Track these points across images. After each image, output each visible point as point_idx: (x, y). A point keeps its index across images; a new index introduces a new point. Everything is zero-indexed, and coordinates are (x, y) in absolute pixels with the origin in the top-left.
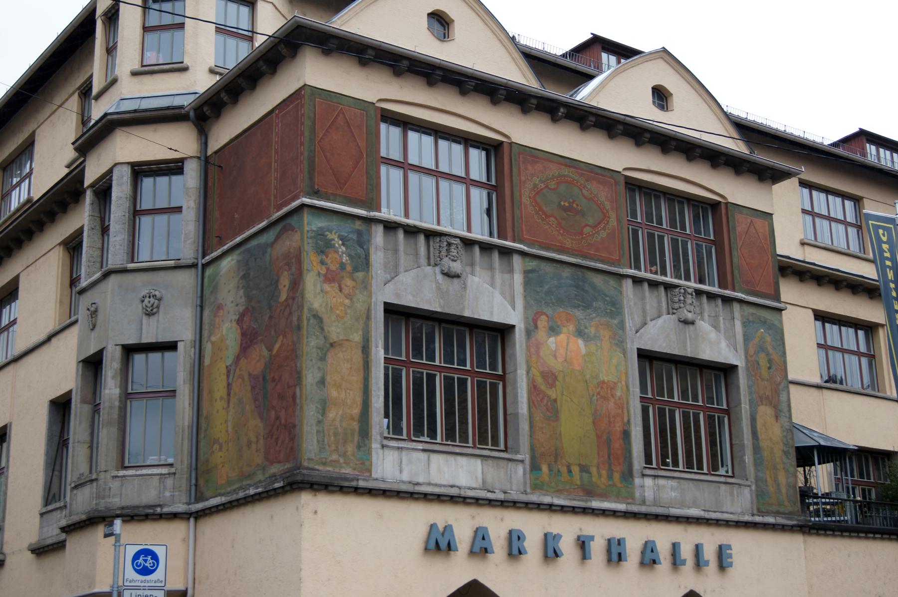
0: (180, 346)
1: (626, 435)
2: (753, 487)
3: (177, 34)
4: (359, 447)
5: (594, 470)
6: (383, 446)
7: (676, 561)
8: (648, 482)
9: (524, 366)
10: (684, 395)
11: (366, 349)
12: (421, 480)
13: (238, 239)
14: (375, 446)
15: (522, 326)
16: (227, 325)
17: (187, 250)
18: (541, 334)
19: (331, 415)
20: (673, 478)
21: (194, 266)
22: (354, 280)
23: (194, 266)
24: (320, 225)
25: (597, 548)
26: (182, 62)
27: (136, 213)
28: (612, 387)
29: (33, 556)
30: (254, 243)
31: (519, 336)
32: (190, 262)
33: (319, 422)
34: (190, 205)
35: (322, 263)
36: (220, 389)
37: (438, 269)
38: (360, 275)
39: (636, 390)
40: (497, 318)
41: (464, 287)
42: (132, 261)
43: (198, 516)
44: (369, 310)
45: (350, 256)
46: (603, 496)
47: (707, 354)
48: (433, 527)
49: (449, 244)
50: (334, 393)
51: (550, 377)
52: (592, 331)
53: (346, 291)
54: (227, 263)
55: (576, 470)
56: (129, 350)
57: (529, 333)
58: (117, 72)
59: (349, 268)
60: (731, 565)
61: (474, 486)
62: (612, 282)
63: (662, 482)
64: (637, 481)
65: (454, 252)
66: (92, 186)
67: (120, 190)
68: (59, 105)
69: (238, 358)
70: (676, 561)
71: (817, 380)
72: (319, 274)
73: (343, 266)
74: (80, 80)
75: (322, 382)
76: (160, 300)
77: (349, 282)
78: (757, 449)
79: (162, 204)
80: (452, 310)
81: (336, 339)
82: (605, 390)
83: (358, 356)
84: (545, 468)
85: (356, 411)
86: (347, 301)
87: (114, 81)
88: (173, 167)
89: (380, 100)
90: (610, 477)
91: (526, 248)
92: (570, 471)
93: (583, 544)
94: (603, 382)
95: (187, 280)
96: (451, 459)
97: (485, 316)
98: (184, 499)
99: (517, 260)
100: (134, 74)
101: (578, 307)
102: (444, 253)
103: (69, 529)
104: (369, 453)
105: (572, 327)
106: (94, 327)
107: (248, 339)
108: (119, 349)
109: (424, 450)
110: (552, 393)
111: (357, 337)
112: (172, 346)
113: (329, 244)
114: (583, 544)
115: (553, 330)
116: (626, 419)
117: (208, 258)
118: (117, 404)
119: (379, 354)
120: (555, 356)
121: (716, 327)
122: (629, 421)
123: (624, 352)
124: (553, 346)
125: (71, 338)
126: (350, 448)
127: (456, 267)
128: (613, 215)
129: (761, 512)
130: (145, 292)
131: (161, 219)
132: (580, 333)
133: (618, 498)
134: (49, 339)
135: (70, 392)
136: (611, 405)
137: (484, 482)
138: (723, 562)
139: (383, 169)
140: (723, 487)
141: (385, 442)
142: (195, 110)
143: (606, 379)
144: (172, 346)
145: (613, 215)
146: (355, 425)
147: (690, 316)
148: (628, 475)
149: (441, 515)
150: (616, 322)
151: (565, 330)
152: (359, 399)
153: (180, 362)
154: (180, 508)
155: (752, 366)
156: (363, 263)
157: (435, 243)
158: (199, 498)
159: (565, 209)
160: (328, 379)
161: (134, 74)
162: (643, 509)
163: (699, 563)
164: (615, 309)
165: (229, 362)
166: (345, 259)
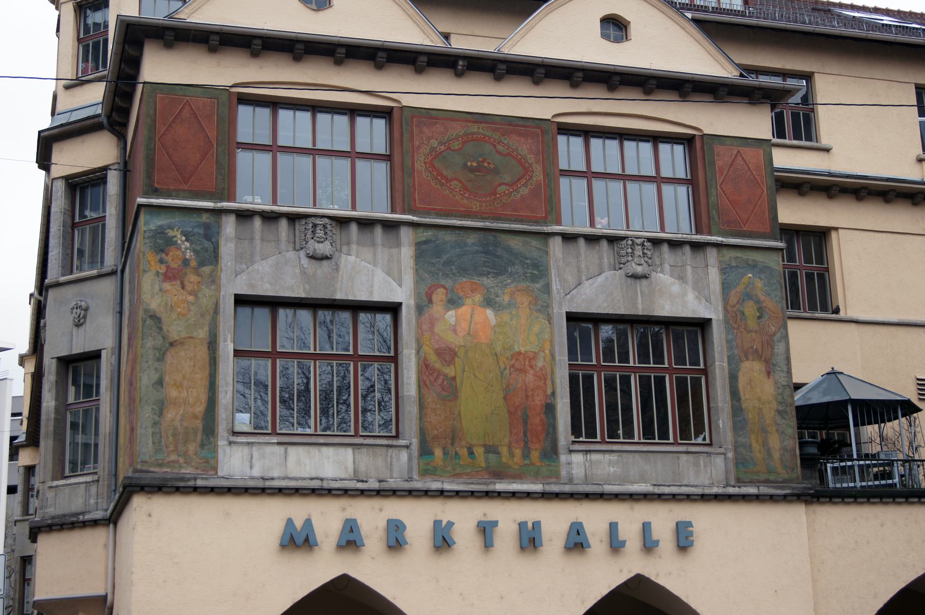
1: (550, 409)
2: (730, 455)
4: (202, 446)
5: (504, 450)
6: (230, 443)
7: (616, 545)
8: (577, 458)
11: (212, 345)
12: (275, 474)
14: (222, 443)
15: (412, 302)
18: (437, 308)
25: (506, 533)
28: (531, 358)
33: (155, 424)
35: (161, 261)
38: (207, 270)
39: (562, 358)
41: (337, 269)
44: (217, 305)
45: (194, 251)
47: (666, 309)
49: (315, 226)
51: (448, 354)
53: (189, 287)
55: (479, 451)
57: (420, 309)
59: (194, 263)
62: (534, 242)
63: (595, 457)
64: (563, 458)
65: (320, 233)
70: (616, 545)
73: (186, 262)
75: (160, 383)
77: (193, 278)
78: (737, 410)
83: (202, 353)
84: (438, 452)
85: (200, 409)
86: (191, 298)
90: (526, 454)
91: (415, 218)
92: (471, 453)
93: (486, 530)
94: (520, 353)
96: (314, 450)
101: (487, 274)
102: (309, 235)
105: (478, 298)
109: (278, 443)
110: (450, 371)
113: (170, 242)
114: (486, 530)
115: (453, 302)
120: (455, 331)
121: (682, 278)
122: (553, 393)
123: (549, 319)
126: (192, 447)
127: (324, 248)
129: (740, 482)
133: (536, 477)
136: (530, 377)
140: (684, 457)
143: (523, 350)
146: (199, 424)
147: (639, 270)
148: (551, 452)
151: (468, 301)
152: (204, 397)
155: (733, 317)
156: (213, 257)
157: (300, 226)
159: (472, 170)
162: (567, 489)
163: (649, 546)
166: (189, 254)
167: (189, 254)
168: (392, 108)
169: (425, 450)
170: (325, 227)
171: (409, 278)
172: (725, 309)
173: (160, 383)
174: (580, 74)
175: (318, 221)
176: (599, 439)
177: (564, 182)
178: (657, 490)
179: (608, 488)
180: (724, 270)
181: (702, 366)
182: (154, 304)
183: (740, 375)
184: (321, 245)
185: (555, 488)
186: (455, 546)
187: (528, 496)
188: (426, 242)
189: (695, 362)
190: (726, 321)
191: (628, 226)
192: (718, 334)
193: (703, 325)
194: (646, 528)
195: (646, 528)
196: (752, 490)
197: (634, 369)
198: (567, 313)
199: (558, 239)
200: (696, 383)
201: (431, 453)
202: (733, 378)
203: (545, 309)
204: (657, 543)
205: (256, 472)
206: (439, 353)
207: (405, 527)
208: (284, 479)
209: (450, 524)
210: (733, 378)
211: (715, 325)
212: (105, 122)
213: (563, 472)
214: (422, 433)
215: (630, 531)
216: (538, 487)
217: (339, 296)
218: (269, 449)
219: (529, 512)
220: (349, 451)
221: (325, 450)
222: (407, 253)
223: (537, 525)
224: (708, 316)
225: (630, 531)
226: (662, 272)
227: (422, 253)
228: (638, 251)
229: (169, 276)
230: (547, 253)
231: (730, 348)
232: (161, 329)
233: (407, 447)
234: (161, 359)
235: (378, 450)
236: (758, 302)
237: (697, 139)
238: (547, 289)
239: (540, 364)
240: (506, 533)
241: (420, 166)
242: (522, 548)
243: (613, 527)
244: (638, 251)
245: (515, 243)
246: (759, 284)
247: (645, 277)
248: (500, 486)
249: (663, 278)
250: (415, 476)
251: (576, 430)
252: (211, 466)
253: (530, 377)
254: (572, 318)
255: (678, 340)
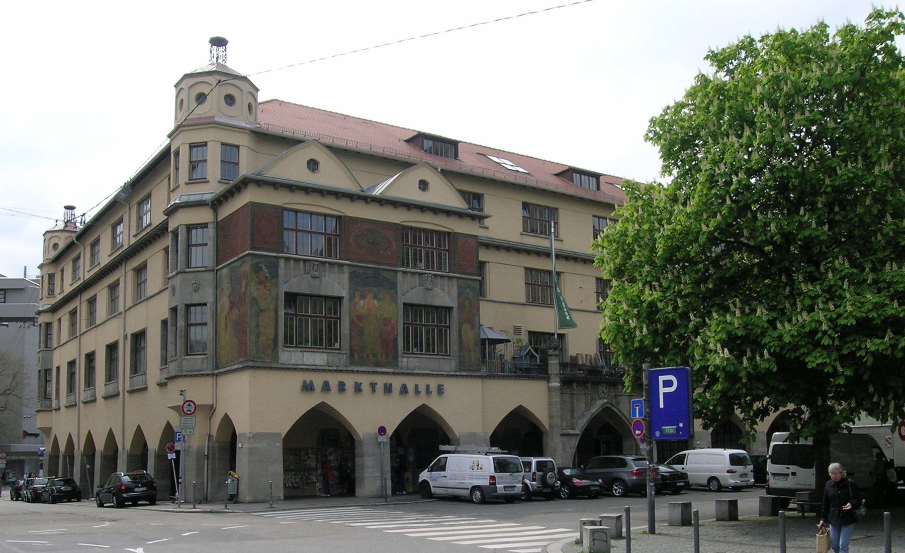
0: (208, 304)
1: (396, 340)
2: (458, 360)
3: (204, 164)
4: (273, 351)
5: (379, 355)
6: (283, 351)
7: (417, 392)
8: (405, 360)
9: (348, 313)
10: (427, 320)
11: (276, 311)
12: (299, 363)
13: (228, 262)
14: (280, 350)
15: (348, 296)
16: (225, 298)
17: (209, 262)
18: (357, 299)
19: (261, 339)
20: (417, 357)
21: (213, 270)
22: (272, 283)
23: (213, 270)
24: (256, 261)
25: (380, 387)
26: (206, 178)
27: (189, 246)
28: (389, 320)
29: (158, 387)
30: (233, 265)
31: (346, 302)
32: (211, 269)
33: (256, 342)
34: (211, 243)
35: (257, 277)
36: (223, 325)
37: (308, 275)
38: (273, 281)
39: (401, 321)
40: (336, 294)
41: (321, 282)
42: (188, 268)
43: (217, 375)
44: (277, 295)
45: (269, 273)
46: (383, 366)
47: (438, 303)
48: (305, 382)
49: (314, 264)
50: (262, 330)
51: (360, 318)
52: (381, 296)
53: (267, 288)
54: (225, 271)
55: (371, 356)
56: (188, 306)
57: (351, 299)
58: (180, 182)
59: (269, 278)
60: (443, 393)
61: (323, 364)
62: (392, 274)
63: (411, 359)
64: (400, 359)
65: (316, 267)
66: (171, 232)
67: (182, 237)
68: (127, 274)
69: (228, 313)
70: (417, 392)
71: (524, 301)
72: (256, 282)
73: (266, 278)
74: (168, 174)
75: (258, 326)
76: (199, 285)
77: (269, 284)
78: (461, 342)
79: (200, 242)
80: (315, 292)
81: (263, 308)
82: (387, 321)
83: (273, 315)
84: (356, 356)
85: (272, 337)
86: (268, 292)
87: (178, 186)
88: (204, 226)
89: (283, 204)
90: (387, 358)
91: (350, 263)
92: (368, 357)
93: (373, 386)
94: (386, 318)
95: (210, 276)
96: (312, 354)
97: (330, 294)
98: (211, 368)
99: (346, 269)
100: (186, 184)
101: (375, 286)
102: (311, 268)
103: (170, 378)
104: (277, 353)
105: (371, 295)
106: (174, 295)
107: (232, 305)
108: (184, 306)
109: (301, 351)
110: (361, 325)
111: (272, 307)
112: (205, 304)
113: (261, 269)
114: (373, 386)
115: (363, 297)
116: (396, 333)
117: (218, 267)
118: (183, 329)
119: (282, 312)
120: (363, 309)
121: (443, 290)
122: (397, 335)
123: (397, 304)
124: (362, 305)
125: (166, 295)
126: (270, 352)
127: (316, 274)
128: (394, 243)
129: (460, 370)
130: (193, 282)
131: (200, 248)
132: (375, 298)
133: (390, 366)
134: (160, 292)
135: (177, 306)
136: (389, 328)
137: (328, 362)
138: (440, 390)
139: (285, 232)
140: (442, 361)
141: (284, 349)
142: (211, 202)
143: (387, 316)
144: (205, 304)
145: (394, 243)
146: (271, 343)
147: (430, 287)
148: (396, 357)
149: (308, 377)
150: (393, 291)
151: (368, 297)
152: (273, 332)
153: (208, 309)
154: (209, 372)
155: (461, 306)
156: (275, 275)
157: (307, 264)
158: (217, 368)
159: (371, 243)
160: (260, 324)
161: (186, 184)
162: (402, 371)
163: (428, 392)
164: (393, 285)
165: (226, 313)
166: (267, 274)
167: (267, 274)
168: (341, 216)
169: (352, 355)
170: (318, 265)
171: (347, 287)
172: (459, 304)
173: (258, 326)
174: (384, 201)
175: (315, 263)
176: (294, 345)
177: (285, 232)
178: (432, 373)
179: (415, 372)
180: (459, 288)
181: (448, 324)
182: (255, 294)
183: (463, 329)
184: (315, 273)
185: (397, 371)
186: (314, 392)
187: (388, 373)
188: (354, 272)
189: (446, 323)
190: (459, 308)
191: (296, 252)
192: (455, 312)
193: (449, 309)
194: (428, 386)
195: (428, 386)
196: (465, 374)
197: (425, 325)
198: (285, 292)
199: (401, 273)
200: (336, 323)
201: (354, 356)
202: (460, 330)
203: (394, 299)
204: (420, 392)
205: (292, 362)
206: (358, 317)
207: (345, 385)
208: (302, 365)
209: (361, 384)
210: (460, 330)
211: (454, 309)
212: (796, 297)
213: (400, 365)
214: (351, 348)
215: (422, 388)
216: (391, 370)
217: (322, 293)
218: (297, 353)
219: (359, 378)
220: (326, 354)
221: (317, 354)
222: (346, 277)
223: (391, 385)
224: (452, 306)
225: (422, 388)
226: (437, 287)
227: (353, 277)
228: (430, 279)
229: (260, 283)
230: (397, 278)
231: (460, 319)
232: (257, 304)
233: (346, 354)
234: (258, 316)
235: (335, 354)
236: (470, 300)
237: (452, 234)
238: (396, 292)
239: (393, 322)
240: (380, 387)
241: (351, 240)
242: (302, 390)
243: (417, 386)
244: (430, 279)
245: (385, 274)
246: (471, 293)
247: (431, 289)
248: (378, 369)
249: (437, 290)
250: (348, 365)
251: (286, 342)
252: (276, 359)
253: (389, 328)
254: (404, 304)
255: (428, 314)
